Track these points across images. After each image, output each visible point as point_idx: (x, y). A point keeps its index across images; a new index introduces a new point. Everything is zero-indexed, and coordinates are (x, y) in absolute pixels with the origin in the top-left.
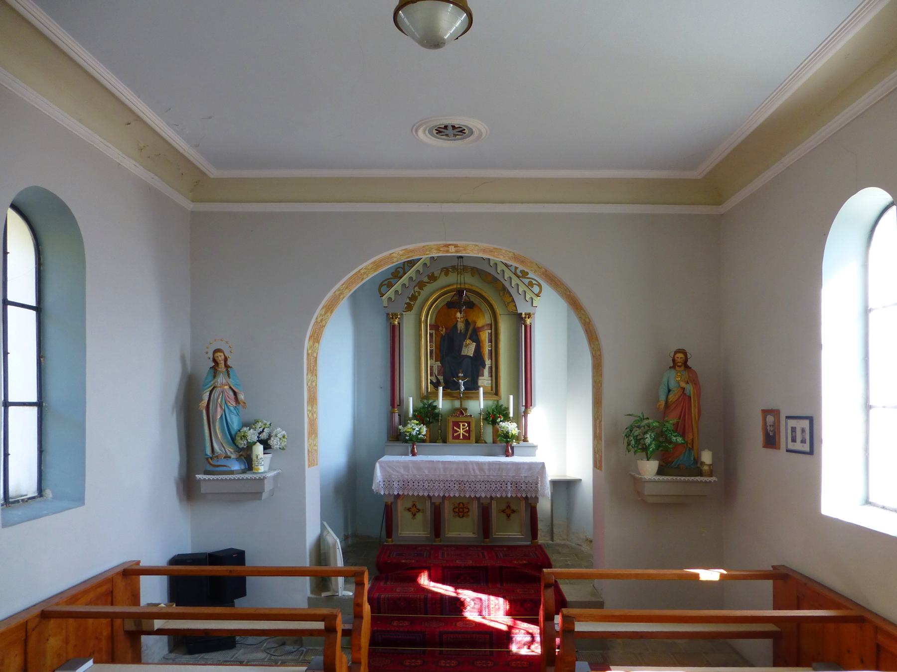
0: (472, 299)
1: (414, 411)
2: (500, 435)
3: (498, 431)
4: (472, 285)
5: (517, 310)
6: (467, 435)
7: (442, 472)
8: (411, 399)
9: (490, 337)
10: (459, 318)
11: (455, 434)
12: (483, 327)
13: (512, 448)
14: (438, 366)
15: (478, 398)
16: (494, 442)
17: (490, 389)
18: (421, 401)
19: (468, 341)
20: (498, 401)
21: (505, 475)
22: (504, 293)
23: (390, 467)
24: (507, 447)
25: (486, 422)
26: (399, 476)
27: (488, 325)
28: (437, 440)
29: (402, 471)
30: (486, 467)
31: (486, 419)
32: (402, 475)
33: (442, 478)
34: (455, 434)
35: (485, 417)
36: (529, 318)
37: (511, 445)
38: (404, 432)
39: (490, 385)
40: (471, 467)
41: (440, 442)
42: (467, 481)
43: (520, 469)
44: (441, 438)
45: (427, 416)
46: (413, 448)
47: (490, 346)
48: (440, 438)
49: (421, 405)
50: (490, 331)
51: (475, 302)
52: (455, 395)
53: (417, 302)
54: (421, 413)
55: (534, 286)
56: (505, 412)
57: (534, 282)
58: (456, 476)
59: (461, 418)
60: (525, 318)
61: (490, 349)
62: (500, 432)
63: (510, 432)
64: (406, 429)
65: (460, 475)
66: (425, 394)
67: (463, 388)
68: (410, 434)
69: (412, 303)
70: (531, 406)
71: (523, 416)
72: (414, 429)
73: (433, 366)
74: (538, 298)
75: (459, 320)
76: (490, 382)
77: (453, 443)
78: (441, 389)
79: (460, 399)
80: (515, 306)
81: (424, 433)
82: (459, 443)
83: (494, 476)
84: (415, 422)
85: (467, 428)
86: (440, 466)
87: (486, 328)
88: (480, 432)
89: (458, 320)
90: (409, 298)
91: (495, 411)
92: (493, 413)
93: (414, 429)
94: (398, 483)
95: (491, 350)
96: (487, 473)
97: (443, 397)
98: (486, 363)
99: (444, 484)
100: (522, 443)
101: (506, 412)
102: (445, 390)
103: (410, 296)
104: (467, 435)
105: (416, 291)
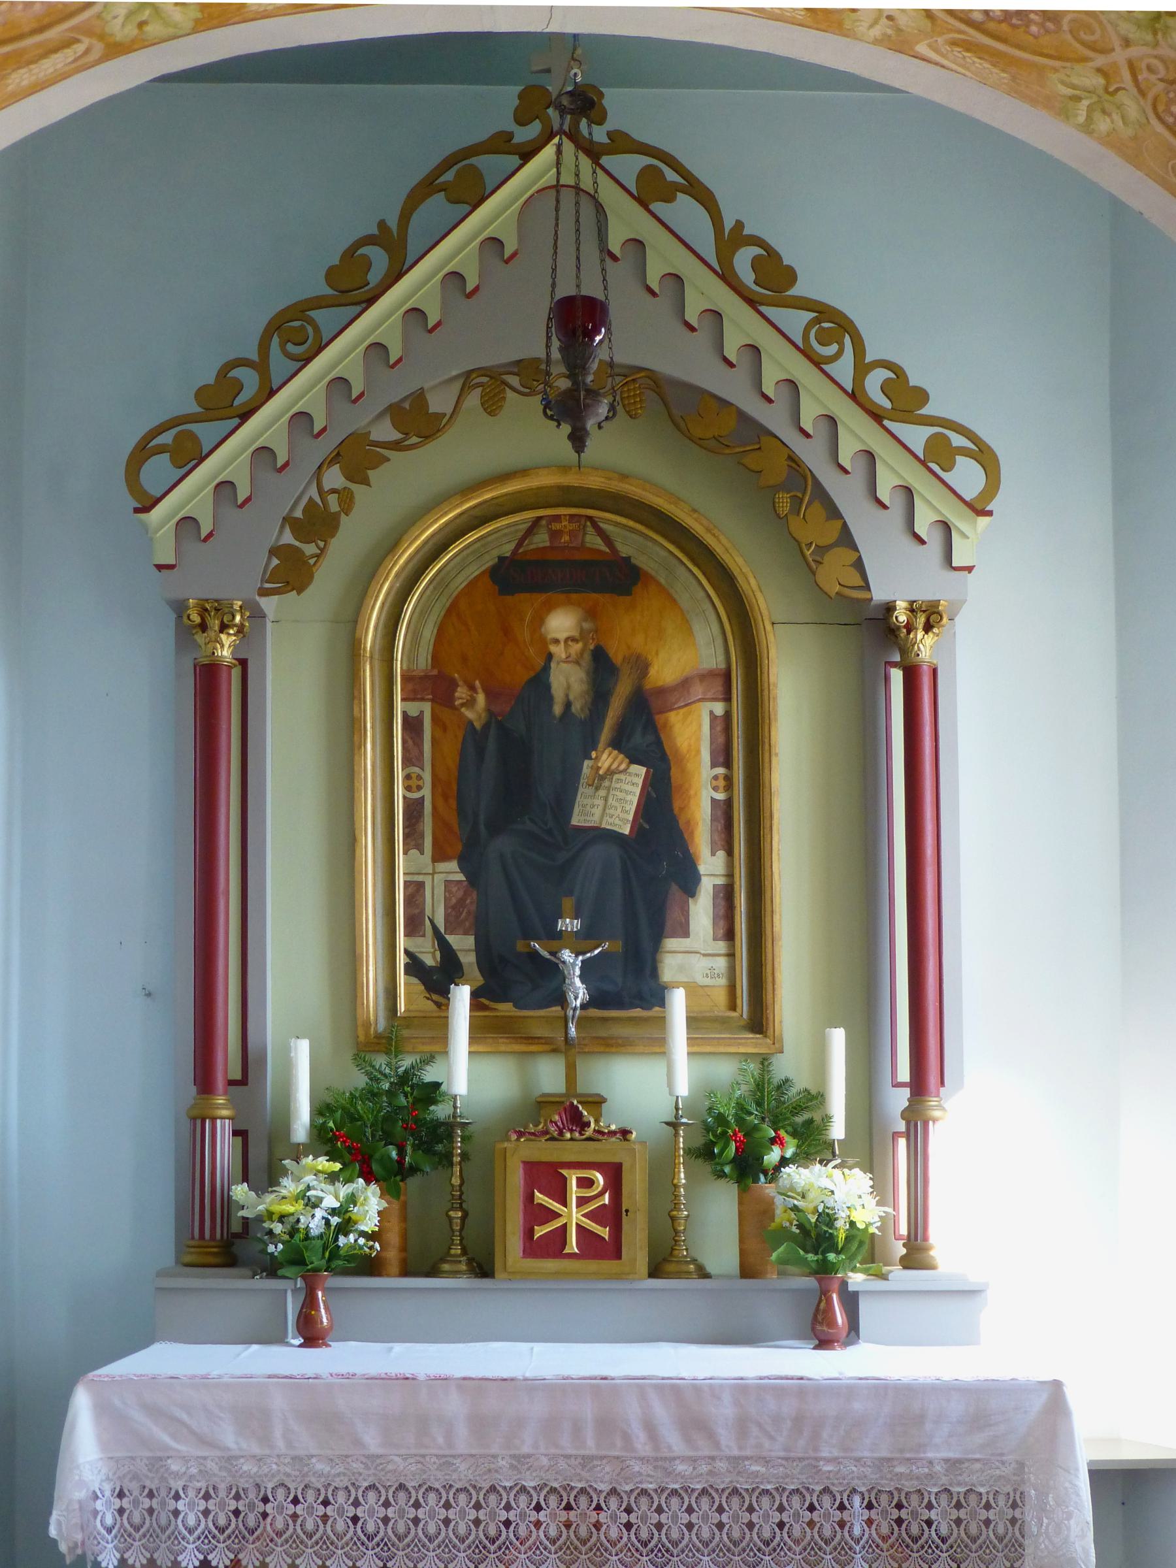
0: (624, 550)
1: (320, 1110)
2: (782, 1235)
3: (766, 1211)
4: (624, 477)
5: (867, 587)
6: (604, 1232)
7: (463, 1442)
8: (302, 1052)
9: (721, 740)
10: (557, 641)
11: (540, 1231)
12: (685, 684)
13: (851, 1301)
14: (447, 883)
15: (658, 1045)
16: (748, 1271)
17: (721, 997)
18: (356, 1057)
19: (607, 759)
20: (764, 1061)
21: (836, 1453)
22: (797, 502)
23: (155, 1412)
24: (825, 1293)
25: (705, 1168)
26: (211, 1465)
27: (710, 675)
28: (443, 1260)
29: (229, 1438)
30: (724, 1412)
31: (705, 1153)
32: (230, 1460)
33: (463, 1473)
34: (540, 1231)
35: (699, 1141)
36: (928, 628)
37: (844, 1284)
38: (259, 1219)
39: (723, 981)
40: (632, 1412)
41: (454, 1274)
42: (613, 1491)
43: (920, 1419)
44: (464, 1252)
45: (388, 1139)
46: (310, 1302)
47: (721, 783)
48: (457, 1250)
49: (360, 1081)
50: (719, 708)
51: (640, 561)
52: (539, 1032)
53: (334, 543)
54: (353, 1117)
55: (960, 459)
56: (799, 1120)
57: (958, 440)
58: (545, 1461)
59: (569, 1149)
60: (910, 628)
61: (721, 796)
62: (782, 1217)
63: (842, 1214)
64: (268, 1202)
65: (568, 1457)
66: (382, 1025)
67: (578, 992)
68: (293, 1232)
69: (310, 549)
70: (942, 1083)
71: (896, 1135)
72: (313, 1204)
73: (421, 885)
74: (983, 521)
75: (558, 651)
76: (721, 963)
77: (526, 1275)
78: (462, 996)
79: (566, 1048)
80: (859, 565)
81: (370, 1223)
82: (557, 1275)
83: (766, 1461)
84: (323, 1163)
85: (606, 1199)
86: (455, 1406)
87: (698, 690)
88: (673, 1219)
89: (553, 648)
90: (288, 520)
91: (753, 1108)
92: (740, 1121)
93: (313, 1204)
94: (202, 1505)
95: (729, 803)
96: (728, 1443)
97: (473, 1039)
98: (702, 869)
99: (478, 1506)
100: (900, 1277)
101: (806, 1116)
102: (484, 1008)
103: (298, 514)
104: (604, 1232)
105: (327, 486)
